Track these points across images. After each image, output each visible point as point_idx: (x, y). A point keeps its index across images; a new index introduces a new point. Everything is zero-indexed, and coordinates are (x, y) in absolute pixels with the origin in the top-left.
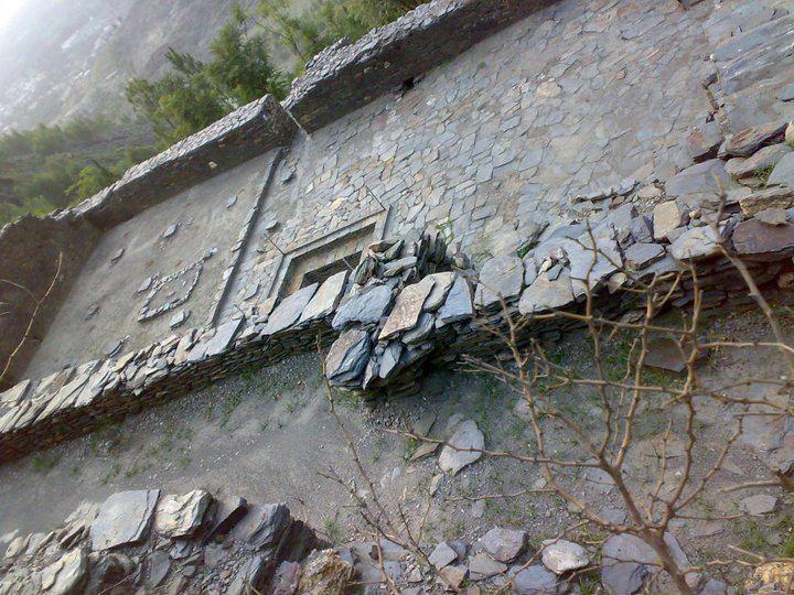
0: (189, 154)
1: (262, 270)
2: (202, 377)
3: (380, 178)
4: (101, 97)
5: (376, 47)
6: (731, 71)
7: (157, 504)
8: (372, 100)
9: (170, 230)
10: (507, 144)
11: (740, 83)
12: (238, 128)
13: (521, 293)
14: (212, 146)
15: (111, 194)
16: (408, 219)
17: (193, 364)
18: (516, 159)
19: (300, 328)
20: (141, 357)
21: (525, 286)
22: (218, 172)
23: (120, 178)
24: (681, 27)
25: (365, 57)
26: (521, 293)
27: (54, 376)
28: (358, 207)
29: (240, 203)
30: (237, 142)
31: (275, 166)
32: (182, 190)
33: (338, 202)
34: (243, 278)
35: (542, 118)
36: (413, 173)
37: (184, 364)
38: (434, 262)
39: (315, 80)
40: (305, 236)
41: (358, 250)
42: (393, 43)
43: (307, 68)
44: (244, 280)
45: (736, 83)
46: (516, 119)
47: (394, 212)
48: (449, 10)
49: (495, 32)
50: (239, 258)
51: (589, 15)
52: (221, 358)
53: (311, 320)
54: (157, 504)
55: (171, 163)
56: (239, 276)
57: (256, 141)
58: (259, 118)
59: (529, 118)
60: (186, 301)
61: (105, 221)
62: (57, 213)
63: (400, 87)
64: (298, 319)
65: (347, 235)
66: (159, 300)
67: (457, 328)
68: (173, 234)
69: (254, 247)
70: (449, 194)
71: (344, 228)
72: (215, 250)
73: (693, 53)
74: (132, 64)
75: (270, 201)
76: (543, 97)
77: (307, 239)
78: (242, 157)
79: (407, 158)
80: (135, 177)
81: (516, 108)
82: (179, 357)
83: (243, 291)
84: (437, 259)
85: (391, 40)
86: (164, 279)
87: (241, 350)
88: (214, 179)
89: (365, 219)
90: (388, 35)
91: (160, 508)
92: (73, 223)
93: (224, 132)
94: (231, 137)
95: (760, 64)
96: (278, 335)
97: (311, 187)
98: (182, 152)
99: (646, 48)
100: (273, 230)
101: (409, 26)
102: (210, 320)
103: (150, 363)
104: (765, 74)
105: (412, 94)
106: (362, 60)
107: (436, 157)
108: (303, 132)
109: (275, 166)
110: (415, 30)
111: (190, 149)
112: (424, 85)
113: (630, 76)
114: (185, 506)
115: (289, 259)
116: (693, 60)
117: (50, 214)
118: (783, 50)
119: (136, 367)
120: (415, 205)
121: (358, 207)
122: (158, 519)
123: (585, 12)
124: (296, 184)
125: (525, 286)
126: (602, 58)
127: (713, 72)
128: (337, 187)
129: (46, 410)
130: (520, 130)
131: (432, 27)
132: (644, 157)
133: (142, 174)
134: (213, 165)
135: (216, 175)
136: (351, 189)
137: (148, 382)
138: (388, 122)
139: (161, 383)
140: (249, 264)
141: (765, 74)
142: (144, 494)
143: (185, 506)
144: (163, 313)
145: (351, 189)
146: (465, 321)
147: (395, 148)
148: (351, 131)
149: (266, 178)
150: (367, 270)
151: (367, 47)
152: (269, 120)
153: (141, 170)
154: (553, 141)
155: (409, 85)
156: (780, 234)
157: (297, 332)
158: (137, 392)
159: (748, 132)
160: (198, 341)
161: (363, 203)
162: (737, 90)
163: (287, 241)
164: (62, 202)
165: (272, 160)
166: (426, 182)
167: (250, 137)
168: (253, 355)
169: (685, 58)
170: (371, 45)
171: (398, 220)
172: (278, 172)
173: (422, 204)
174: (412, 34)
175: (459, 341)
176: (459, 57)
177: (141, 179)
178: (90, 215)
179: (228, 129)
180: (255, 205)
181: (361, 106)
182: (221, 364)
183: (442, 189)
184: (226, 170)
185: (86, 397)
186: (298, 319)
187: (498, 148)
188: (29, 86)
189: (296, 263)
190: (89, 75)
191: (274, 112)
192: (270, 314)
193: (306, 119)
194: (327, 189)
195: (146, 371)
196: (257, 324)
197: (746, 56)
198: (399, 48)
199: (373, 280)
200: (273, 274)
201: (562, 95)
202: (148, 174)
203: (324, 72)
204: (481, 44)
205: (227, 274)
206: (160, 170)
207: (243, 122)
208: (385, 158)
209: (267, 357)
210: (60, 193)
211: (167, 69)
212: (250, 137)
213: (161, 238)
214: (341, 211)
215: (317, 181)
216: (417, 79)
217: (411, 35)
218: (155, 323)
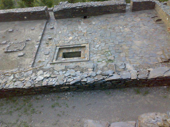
8: (75, 17)
9: (11, 30)
14: (28, 13)
22: (26, 20)
30: (36, 14)
32: (13, 21)
48: (101, 5)
49: (108, 14)
55: (13, 13)
56: (40, 48)
57: (41, 16)
65: (76, 47)
66: (11, 47)
68: (12, 31)
72: (30, 39)
77: (63, 44)
78: (35, 19)
88: (24, 21)
94: (34, 13)
102: (76, 59)
106: (77, 8)
110: (92, 6)
115: (58, 48)
131: (96, 7)
144: (14, 51)
148: (69, 22)
151: (79, 5)
156: (16, 86)
167: (40, 14)
176: (99, 16)
180: (42, 31)
181: (71, 18)
184: (28, 20)
204: (105, 15)
205: (37, 46)
206: (9, 14)
212: (40, 14)
213: (7, 31)
218: (11, 54)
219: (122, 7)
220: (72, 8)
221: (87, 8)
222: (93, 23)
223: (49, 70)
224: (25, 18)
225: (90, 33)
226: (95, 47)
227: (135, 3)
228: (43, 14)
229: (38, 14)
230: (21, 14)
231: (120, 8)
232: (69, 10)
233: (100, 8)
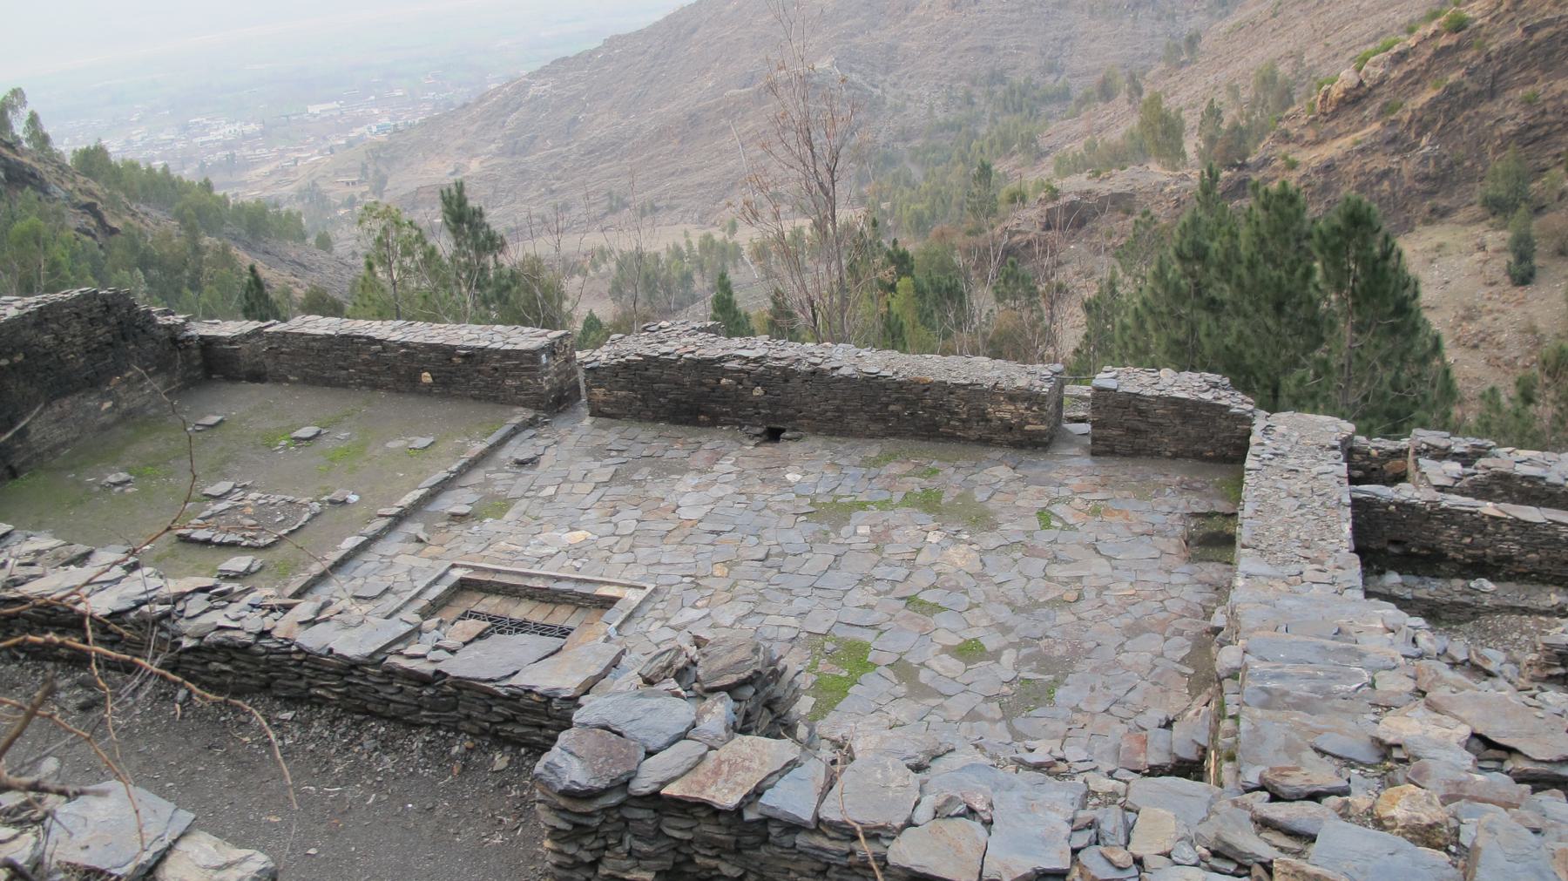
0: (403, 345)
1: (410, 566)
2: (300, 677)
3: (663, 537)
4: (314, 195)
5: (755, 360)
6: (1262, 676)
7: (183, 835)
9: (1198, 485)
10: (873, 600)
11: (1270, 700)
12: (497, 351)
13: (903, 828)
15: (257, 333)
16: (672, 623)
17: (300, 651)
18: (873, 627)
19: (502, 692)
20: (222, 594)
21: (910, 823)
22: (427, 392)
23: (285, 320)
24: (1176, 579)
25: (734, 365)
26: (903, 828)
27: (53, 543)
28: (607, 559)
29: (327, 443)
31: (516, 431)
33: (579, 536)
34: (371, 559)
35: (939, 592)
36: (715, 559)
37: (288, 642)
38: (772, 711)
39: (647, 352)
40: (503, 556)
41: (568, 624)
42: (783, 369)
43: (645, 329)
44: (371, 566)
45: (1265, 696)
46: (901, 573)
47: (658, 598)
50: (384, 529)
51: (1064, 492)
52: (351, 667)
53: (529, 691)
54: (183, 835)
55: (372, 341)
56: (366, 556)
57: (509, 382)
58: (534, 355)
59: (921, 579)
60: (267, 547)
61: (215, 365)
62: (166, 313)
63: (759, 430)
64: (508, 677)
67: (774, 831)
69: (415, 528)
70: (754, 621)
71: (568, 579)
73: (1177, 624)
74: (383, 181)
75: (477, 476)
76: (953, 564)
79: (718, 533)
80: (307, 331)
81: (907, 556)
82: (284, 626)
83: (359, 582)
84: (778, 707)
85: (784, 363)
86: (254, 495)
87: (391, 674)
89: (609, 584)
90: (783, 355)
91: (183, 846)
92: (175, 339)
93: (472, 344)
95: (1302, 689)
96: (462, 684)
97: (550, 491)
98: (396, 336)
99: (1120, 581)
100: (457, 518)
101: (818, 360)
103: (233, 610)
104: (1303, 705)
105: (767, 449)
107: (761, 555)
108: (585, 410)
109: (516, 431)
111: (409, 338)
112: (794, 448)
113: (1082, 604)
114: (228, 865)
115: (458, 574)
116: (1174, 634)
117: (154, 309)
118: (1338, 687)
119: (208, 604)
120: (694, 606)
121: (607, 559)
122: (171, 859)
123: (1061, 485)
124: (529, 474)
125: (910, 823)
126: (1055, 559)
127: (1236, 664)
128: (593, 514)
129: (20, 588)
130: (901, 590)
132: (1052, 727)
133: (320, 331)
134: (427, 377)
135: (420, 393)
136: (608, 528)
137: (213, 637)
138: (716, 467)
139: (232, 651)
140: (392, 546)
141: (1303, 705)
142: (167, 807)
143: (228, 865)
145: (608, 528)
146: (794, 827)
147: (707, 508)
149: (491, 440)
150: (670, 665)
151: (745, 353)
152: (547, 365)
153: (321, 326)
154: (940, 632)
155: (773, 435)
157: (494, 696)
158: (187, 643)
159: (1297, 769)
160: (327, 620)
161: (617, 558)
162: (1265, 706)
163: (469, 547)
164: (170, 294)
165: (516, 420)
166: (727, 583)
167: (505, 372)
168: (401, 690)
169: (1164, 624)
170: (752, 354)
171: (655, 614)
172: (513, 442)
173: (706, 611)
174: (816, 374)
175: (764, 852)
177: (314, 338)
178: (207, 343)
179: (482, 344)
180: (454, 467)
182: (343, 676)
183: (746, 608)
185: (101, 604)
186: (508, 677)
187: (859, 596)
188: (225, 130)
189: (464, 586)
190: (316, 164)
191: (561, 359)
192: (465, 644)
193: (599, 393)
194: (564, 507)
195: (218, 618)
196: (436, 648)
197: (1288, 668)
198: (786, 381)
199: (672, 684)
200: (420, 586)
201: (980, 577)
202: (330, 337)
203: (664, 349)
205: (350, 543)
206: (347, 341)
207: (509, 347)
208: (684, 513)
209: (420, 707)
210: (177, 276)
211: (433, 216)
212: (505, 372)
214: (575, 551)
215: (566, 487)
216: (787, 435)
217: (814, 373)
219: (1022, 406)
220: (699, 361)
221: (787, 375)
222: (789, 477)
223: (680, 675)
224: (427, 377)
225: (712, 532)
226: (667, 619)
227: (1106, 398)
228: (526, 369)
229: (496, 369)
230: (405, 355)
231: (1006, 412)
232: (680, 368)
233: (870, 389)
